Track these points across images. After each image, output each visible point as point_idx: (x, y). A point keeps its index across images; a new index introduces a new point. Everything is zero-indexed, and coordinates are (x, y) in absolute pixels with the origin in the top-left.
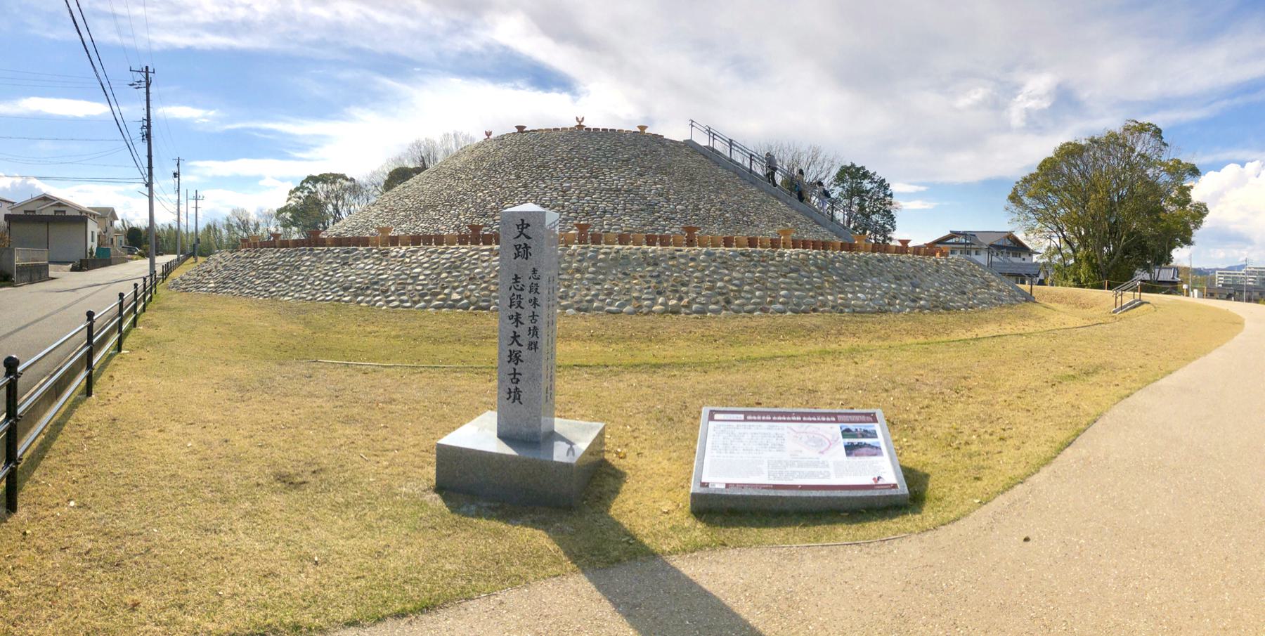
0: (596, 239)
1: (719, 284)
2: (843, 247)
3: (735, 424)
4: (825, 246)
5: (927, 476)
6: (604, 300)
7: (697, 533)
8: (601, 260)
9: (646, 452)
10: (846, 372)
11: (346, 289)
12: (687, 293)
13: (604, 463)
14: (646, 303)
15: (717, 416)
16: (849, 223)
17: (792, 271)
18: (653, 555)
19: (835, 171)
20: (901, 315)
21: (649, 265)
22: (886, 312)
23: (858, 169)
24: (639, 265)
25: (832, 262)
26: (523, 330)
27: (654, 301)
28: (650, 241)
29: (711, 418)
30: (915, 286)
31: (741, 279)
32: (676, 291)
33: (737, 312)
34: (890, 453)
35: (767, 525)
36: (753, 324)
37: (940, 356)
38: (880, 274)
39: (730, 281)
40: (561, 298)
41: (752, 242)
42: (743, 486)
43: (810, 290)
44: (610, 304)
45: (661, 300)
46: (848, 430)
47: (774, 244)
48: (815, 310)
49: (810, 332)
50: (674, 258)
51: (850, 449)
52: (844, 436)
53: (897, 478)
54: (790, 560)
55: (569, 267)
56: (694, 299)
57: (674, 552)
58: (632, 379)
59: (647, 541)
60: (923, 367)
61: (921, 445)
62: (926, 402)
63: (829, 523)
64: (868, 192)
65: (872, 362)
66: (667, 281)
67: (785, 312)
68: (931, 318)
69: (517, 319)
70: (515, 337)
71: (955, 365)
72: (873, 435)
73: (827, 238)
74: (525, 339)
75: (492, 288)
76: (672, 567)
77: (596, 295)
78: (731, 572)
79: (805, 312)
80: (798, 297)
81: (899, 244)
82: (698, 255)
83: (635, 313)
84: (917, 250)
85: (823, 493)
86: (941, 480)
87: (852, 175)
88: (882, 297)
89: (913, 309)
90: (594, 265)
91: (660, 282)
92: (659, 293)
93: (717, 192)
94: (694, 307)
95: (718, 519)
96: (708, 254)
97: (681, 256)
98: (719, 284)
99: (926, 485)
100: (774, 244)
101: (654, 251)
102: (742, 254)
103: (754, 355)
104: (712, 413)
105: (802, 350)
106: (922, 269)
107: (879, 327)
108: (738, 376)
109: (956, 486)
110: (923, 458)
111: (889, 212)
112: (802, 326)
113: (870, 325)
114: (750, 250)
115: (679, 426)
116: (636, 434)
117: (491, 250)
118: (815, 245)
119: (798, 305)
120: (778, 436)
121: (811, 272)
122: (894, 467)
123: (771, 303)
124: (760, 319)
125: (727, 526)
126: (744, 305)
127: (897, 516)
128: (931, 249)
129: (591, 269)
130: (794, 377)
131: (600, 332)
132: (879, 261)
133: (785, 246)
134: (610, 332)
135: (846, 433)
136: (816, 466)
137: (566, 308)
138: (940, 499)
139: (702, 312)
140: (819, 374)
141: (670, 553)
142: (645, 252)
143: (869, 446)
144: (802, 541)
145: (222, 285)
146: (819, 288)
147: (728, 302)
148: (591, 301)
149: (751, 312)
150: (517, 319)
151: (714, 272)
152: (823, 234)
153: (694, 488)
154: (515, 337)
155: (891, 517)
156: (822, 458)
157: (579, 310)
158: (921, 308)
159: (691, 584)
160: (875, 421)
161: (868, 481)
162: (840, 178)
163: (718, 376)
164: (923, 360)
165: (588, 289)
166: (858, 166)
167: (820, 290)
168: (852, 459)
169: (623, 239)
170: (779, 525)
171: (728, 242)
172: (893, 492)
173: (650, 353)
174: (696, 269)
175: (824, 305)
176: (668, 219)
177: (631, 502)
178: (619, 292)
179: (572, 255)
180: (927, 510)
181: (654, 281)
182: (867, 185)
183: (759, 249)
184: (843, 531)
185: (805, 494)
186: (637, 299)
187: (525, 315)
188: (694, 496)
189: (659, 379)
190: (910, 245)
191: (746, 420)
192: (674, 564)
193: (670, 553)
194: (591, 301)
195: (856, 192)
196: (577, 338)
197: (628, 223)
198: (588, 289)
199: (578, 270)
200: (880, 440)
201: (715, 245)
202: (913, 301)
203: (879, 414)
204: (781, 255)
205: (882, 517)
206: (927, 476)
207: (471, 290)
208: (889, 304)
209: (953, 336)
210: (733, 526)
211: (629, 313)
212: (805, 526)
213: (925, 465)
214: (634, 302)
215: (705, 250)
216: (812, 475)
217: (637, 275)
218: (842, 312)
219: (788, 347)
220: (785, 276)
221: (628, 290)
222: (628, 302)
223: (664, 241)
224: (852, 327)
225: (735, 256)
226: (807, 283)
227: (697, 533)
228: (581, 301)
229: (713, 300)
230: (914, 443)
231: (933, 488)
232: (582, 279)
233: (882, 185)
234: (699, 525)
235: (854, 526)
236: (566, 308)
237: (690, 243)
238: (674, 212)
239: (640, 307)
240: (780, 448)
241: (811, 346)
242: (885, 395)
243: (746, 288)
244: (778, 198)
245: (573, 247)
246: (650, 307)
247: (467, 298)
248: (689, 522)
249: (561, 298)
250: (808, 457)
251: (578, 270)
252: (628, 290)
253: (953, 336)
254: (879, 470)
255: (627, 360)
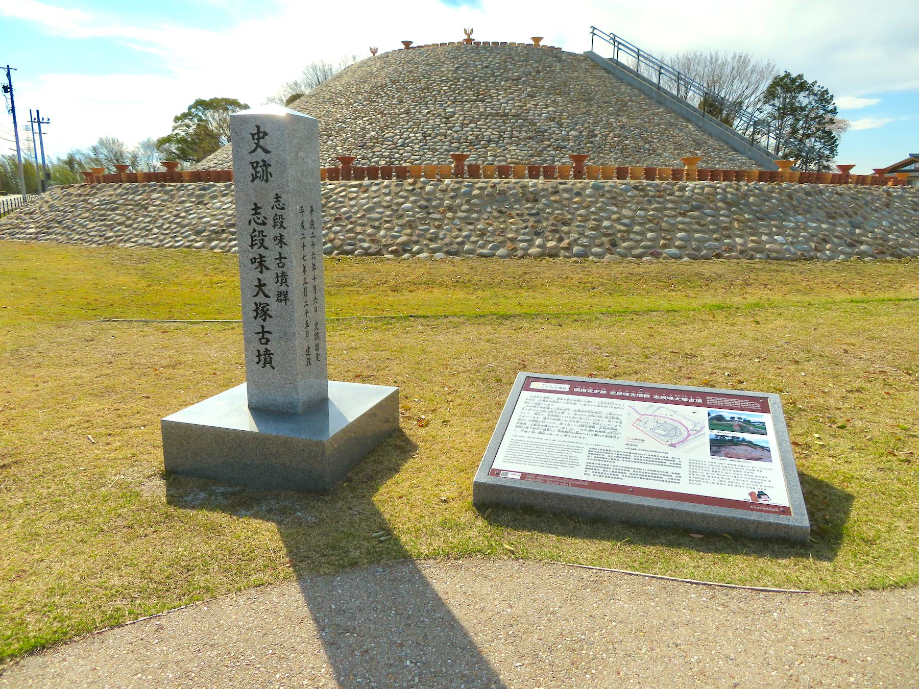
0: (474, 172)
1: (606, 223)
2: (762, 177)
3: (555, 396)
4: (739, 176)
5: (849, 498)
6: (476, 242)
7: (475, 531)
8: (476, 197)
9: (454, 421)
10: (742, 334)
11: (198, 233)
12: (568, 233)
13: (398, 433)
14: (521, 245)
15: (534, 385)
16: (777, 149)
17: (694, 209)
18: (404, 558)
19: (764, 86)
20: (831, 263)
21: (528, 201)
22: (811, 259)
23: (793, 81)
24: (517, 201)
25: (746, 196)
26: (268, 277)
27: (530, 242)
28: (534, 173)
29: (526, 387)
30: (855, 227)
31: (632, 218)
32: (556, 231)
33: (624, 256)
34: (783, 459)
35: (573, 533)
36: (641, 270)
37: (885, 320)
38: (808, 210)
39: (618, 219)
40: (430, 240)
41: (650, 174)
42: (546, 479)
43: (714, 231)
44: (482, 247)
45: (538, 241)
46: (720, 418)
47: (677, 175)
48: (718, 256)
49: (709, 281)
50: (556, 192)
51: (718, 446)
52: (712, 426)
53: (791, 498)
54: (596, 591)
55: (440, 205)
56: (576, 240)
57: (434, 556)
58: (471, 331)
59: (404, 538)
60: (856, 333)
61: (844, 445)
62: (857, 384)
63: (670, 544)
64: (803, 109)
65: (780, 322)
66: (547, 219)
67: (680, 257)
68: (872, 267)
69: (260, 262)
70: (261, 285)
71: (907, 333)
72: (761, 429)
73: (744, 168)
74: (272, 287)
75: (359, 229)
76: (422, 577)
77: (468, 237)
78: (496, 596)
79: (706, 258)
80: (698, 240)
81: (838, 172)
82: (584, 188)
83: (508, 256)
84: (861, 180)
85: (667, 504)
86: (875, 508)
87: (788, 86)
88: (807, 240)
89: (849, 255)
90: (468, 202)
91: (539, 221)
92: (538, 234)
93: (617, 115)
94: (576, 249)
95: (506, 517)
96: (596, 188)
97: (565, 190)
98: (606, 223)
99: (847, 513)
100: (677, 175)
101: (535, 185)
102: (635, 188)
103: (636, 307)
104: (529, 380)
105: (695, 304)
106: (867, 204)
107: (798, 277)
108: (598, 332)
109: (901, 524)
110: (845, 468)
111: (830, 132)
112: (699, 275)
113: (787, 274)
114: (645, 182)
115: (492, 391)
116: (450, 398)
117: (360, 186)
118: (727, 175)
119: (698, 249)
120: (611, 417)
121: (718, 209)
122: (787, 477)
123: (665, 246)
124: (649, 265)
125: (516, 529)
126: (632, 248)
127: (785, 556)
128: (881, 177)
129: (465, 207)
130: (669, 336)
131: (468, 278)
132: (808, 194)
133: (690, 178)
134: (477, 278)
135: (716, 422)
136: (662, 463)
137: (434, 251)
138: (870, 542)
139: (583, 255)
140: (704, 334)
141: (427, 557)
142: (524, 187)
143: (750, 444)
144: (622, 565)
145: (46, 230)
146: (726, 228)
147: (614, 244)
148: (462, 243)
149: (639, 256)
150: (260, 262)
151: (601, 209)
152: (740, 162)
153: (481, 476)
154: (261, 285)
155: (776, 555)
156: (672, 453)
157: (448, 253)
158: (861, 255)
159: (439, 603)
160: (765, 409)
161: (741, 494)
162: (770, 94)
163: (573, 330)
164: (857, 324)
165: (460, 230)
166: (794, 75)
167: (727, 233)
168: (717, 460)
169: (503, 172)
170: (591, 535)
171: (621, 173)
172: (783, 520)
173: (509, 302)
174: (580, 205)
175: (731, 249)
176: (559, 148)
177: (407, 484)
178: (493, 233)
179: (444, 191)
180: (844, 553)
181: (533, 219)
182: (803, 99)
183: (657, 181)
184: (688, 560)
185: (636, 500)
186: (512, 240)
187: (271, 259)
188: (477, 486)
189: (503, 333)
190: (852, 172)
191: (571, 392)
192: (426, 572)
193: (427, 557)
194: (462, 243)
195: (789, 110)
196: (441, 285)
197: (515, 154)
198: (460, 230)
199: (450, 208)
200: (770, 440)
201: (607, 177)
202: (850, 245)
203: (774, 400)
204: (682, 189)
205: (760, 553)
206: (849, 498)
207: (336, 233)
208: (816, 249)
209: (904, 293)
210: (524, 528)
211: (502, 257)
212: (631, 542)
213: (848, 479)
214: (509, 244)
215: (593, 182)
216: (653, 475)
217: (514, 213)
218: (752, 258)
219: (679, 300)
220: (684, 215)
221: (504, 231)
222: (502, 244)
223: (549, 173)
224: (764, 276)
225: (627, 191)
226: (711, 223)
227: (475, 531)
228: (451, 243)
229: (597, 241)
230: (832, 442)
231: (858, 518)
232: (453, 218)
233: (824, 98)
234: (480, 523)
235: (709, 556)
236: (434, 251)
237: (578, 175)
238: (566, 139)
239: (515, 249)
240: (613, 433)
241: (709, 298)
242: (793, 367)
243: (637, 228)
244: (688, 121)
245: (447, 181)
246: (526, 249)
247: (331, 241)
248: (466, 517)
249: (430, 240)
250: (661, 450)
251: (450, 208)
252: (504, 231)
253: (904, 293)
254: (767, 482)
255: (488, 307)
